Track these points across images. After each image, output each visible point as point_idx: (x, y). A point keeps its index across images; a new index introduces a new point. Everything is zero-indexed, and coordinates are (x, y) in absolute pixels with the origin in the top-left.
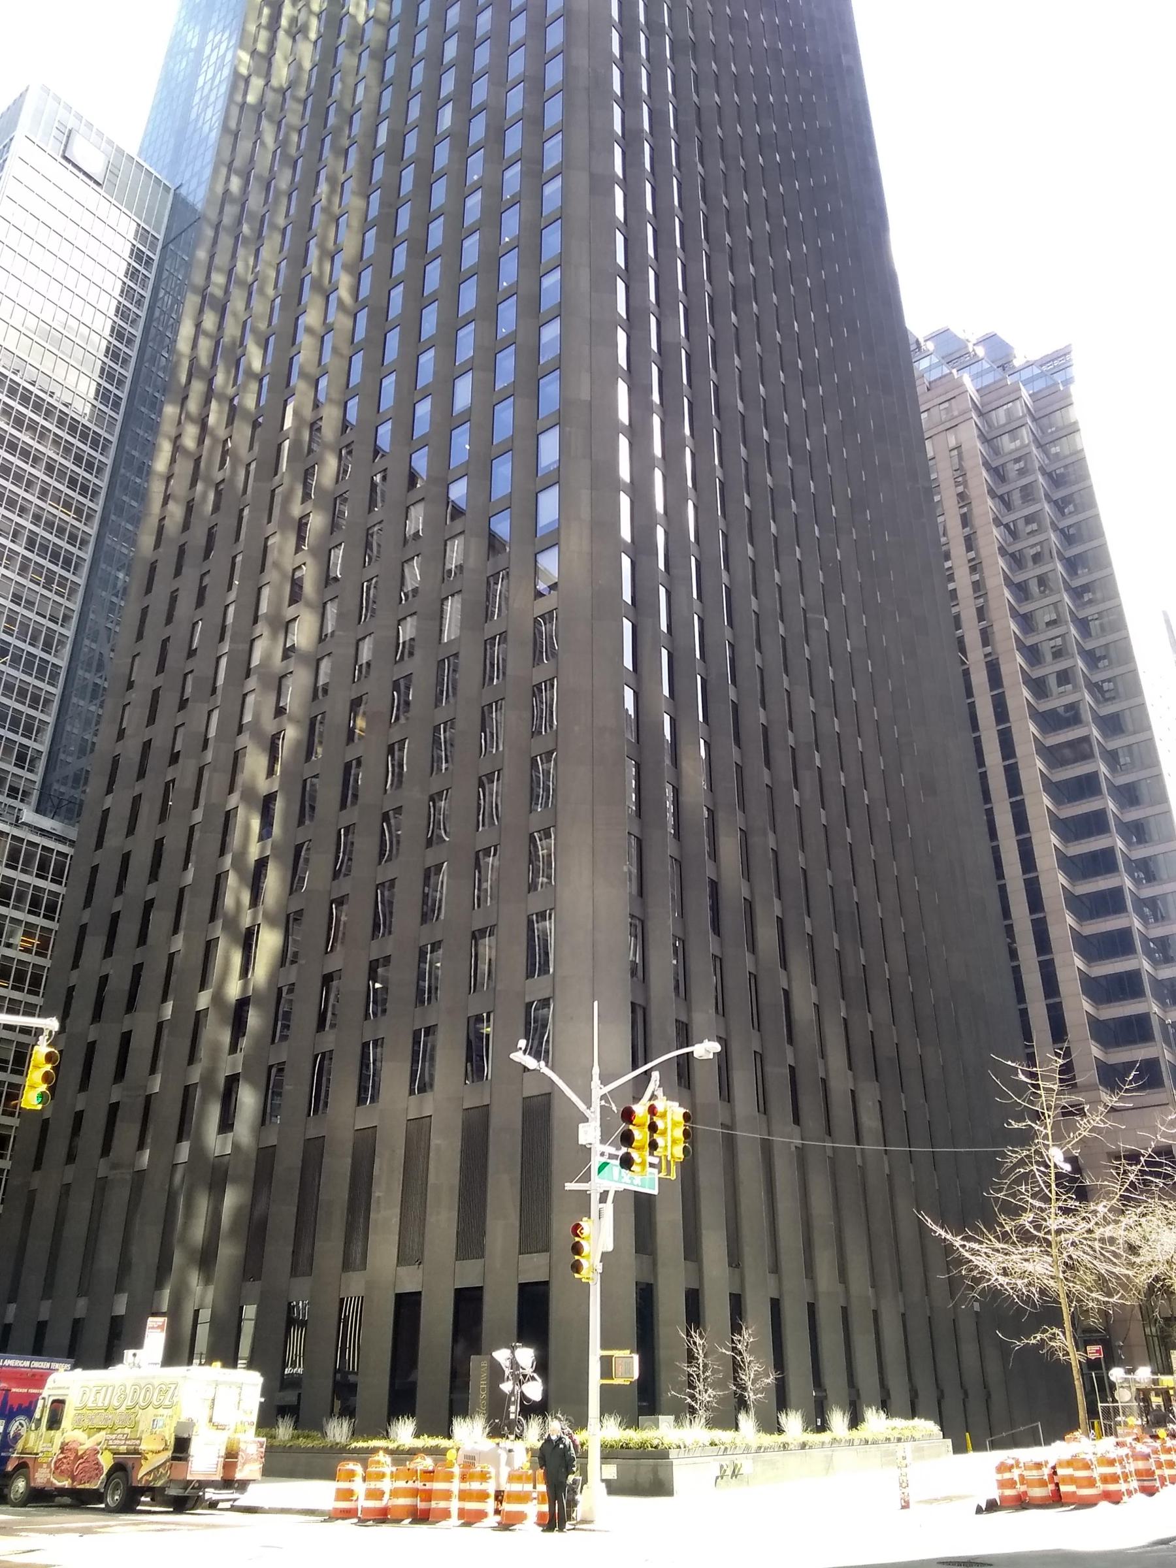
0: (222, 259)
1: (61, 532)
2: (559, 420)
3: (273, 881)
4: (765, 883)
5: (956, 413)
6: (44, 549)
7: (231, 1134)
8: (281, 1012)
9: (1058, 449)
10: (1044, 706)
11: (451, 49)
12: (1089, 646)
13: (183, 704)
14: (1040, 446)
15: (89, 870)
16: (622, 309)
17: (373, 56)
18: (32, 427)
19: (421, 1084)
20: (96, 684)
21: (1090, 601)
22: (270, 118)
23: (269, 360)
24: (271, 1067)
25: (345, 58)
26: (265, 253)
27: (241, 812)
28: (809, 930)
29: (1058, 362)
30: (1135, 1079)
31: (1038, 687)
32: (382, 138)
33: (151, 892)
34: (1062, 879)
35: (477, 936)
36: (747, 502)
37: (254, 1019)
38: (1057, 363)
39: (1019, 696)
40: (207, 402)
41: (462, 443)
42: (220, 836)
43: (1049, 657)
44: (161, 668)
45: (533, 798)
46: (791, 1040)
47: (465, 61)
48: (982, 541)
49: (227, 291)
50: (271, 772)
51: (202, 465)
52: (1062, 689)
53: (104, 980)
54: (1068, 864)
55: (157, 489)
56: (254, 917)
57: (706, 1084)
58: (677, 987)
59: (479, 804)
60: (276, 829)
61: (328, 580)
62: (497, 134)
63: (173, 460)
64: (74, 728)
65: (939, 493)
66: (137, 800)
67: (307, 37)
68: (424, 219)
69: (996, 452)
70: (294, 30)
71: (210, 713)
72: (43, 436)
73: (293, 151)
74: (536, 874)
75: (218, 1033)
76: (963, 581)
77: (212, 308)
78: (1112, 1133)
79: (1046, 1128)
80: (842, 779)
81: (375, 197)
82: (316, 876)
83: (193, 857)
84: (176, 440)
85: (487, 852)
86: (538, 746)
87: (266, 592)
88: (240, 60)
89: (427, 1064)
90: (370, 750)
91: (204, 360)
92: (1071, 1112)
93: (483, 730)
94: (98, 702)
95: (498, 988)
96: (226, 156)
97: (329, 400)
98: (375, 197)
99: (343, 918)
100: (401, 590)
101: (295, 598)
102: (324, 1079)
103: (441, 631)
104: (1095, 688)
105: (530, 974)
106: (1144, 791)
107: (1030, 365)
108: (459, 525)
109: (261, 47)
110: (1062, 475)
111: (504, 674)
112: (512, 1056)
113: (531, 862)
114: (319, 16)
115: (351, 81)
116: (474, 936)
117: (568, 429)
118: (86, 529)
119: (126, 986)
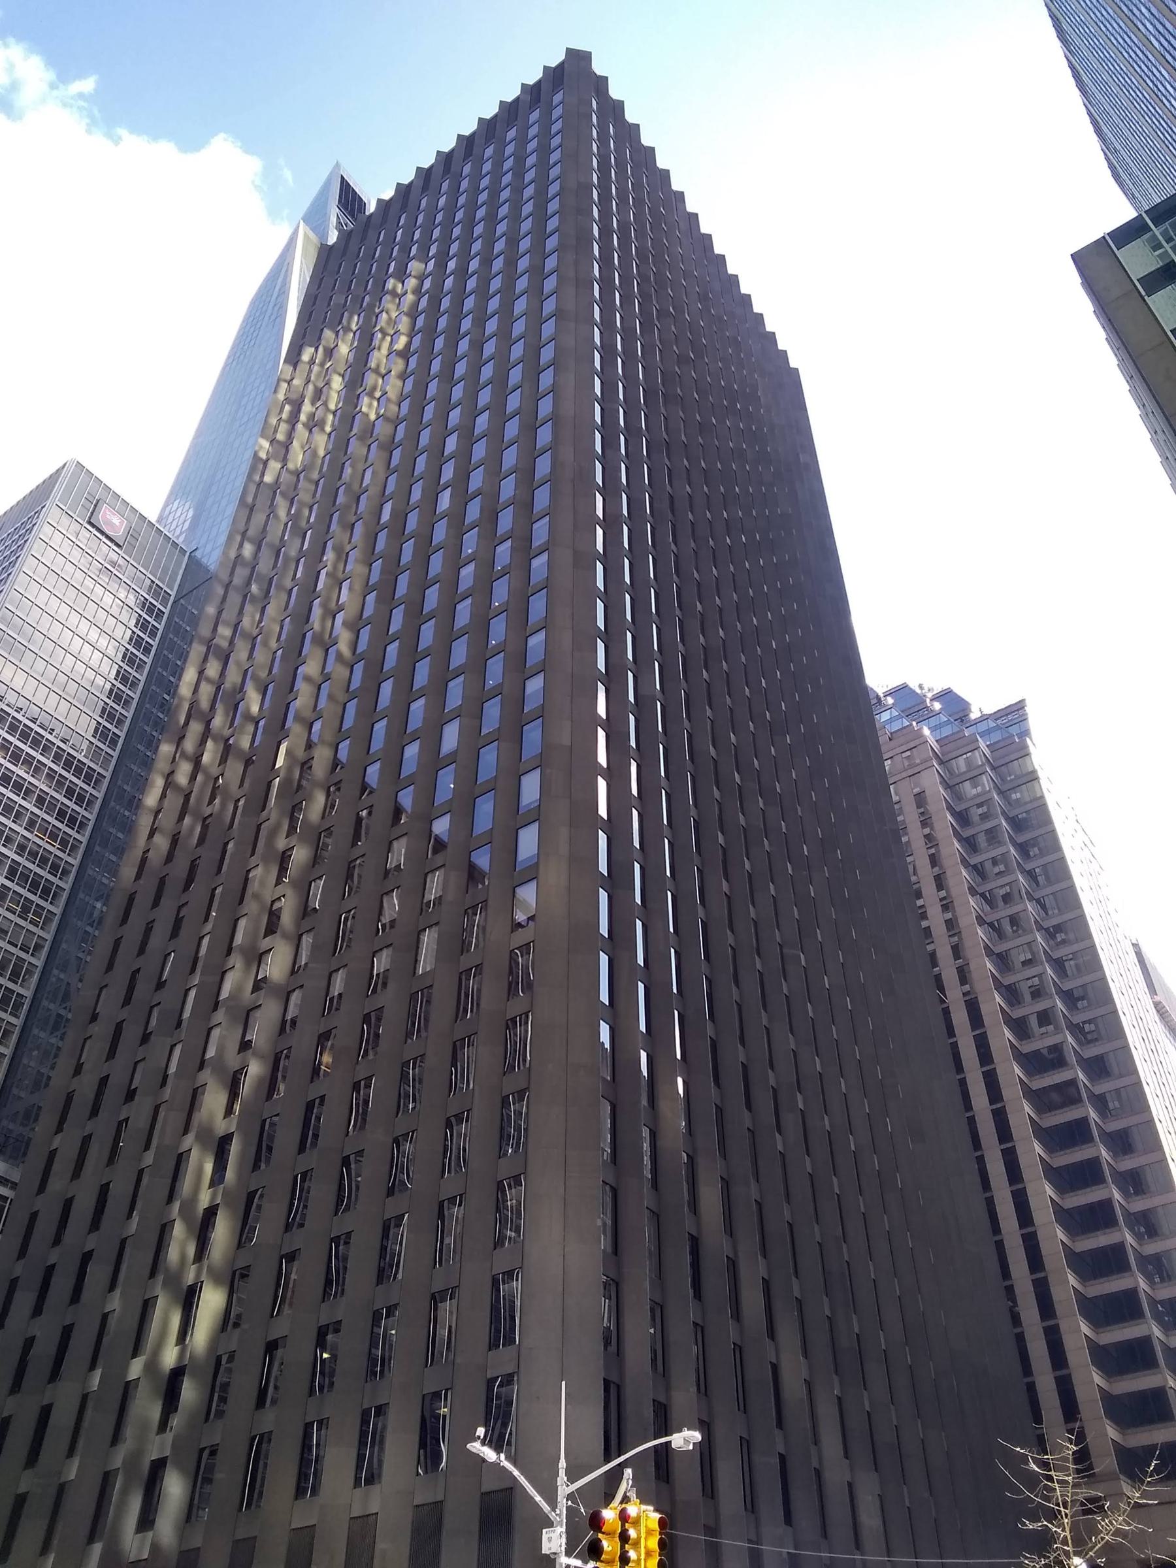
0: (229, 614)
1: (43, 862)
2: (540, 763)
3: (222, 1232)
4: (748, 1244)
5: (918, 761)
6: (24, 878)
7: (150, 1534)
8: (218, 1383)
9: (1018, 795)
10: (1027, 1048)
11: (451, 444)
12: (1067, 986)
13: (145, 1038)
14: (1001, 793)
15: (28, 1216)
16: (601, 666)
17: (381, 447)
18: (28, 761)
19: (367, 1474)
20: (59, 1015)
21: (1064, 942)
22: (283, 494)
23: (267, 705)
24: (202, 1450)
25: (355, 447)
26: (271, 610)
27: (194, 1154)
28: (797, 1293)
29: (1014, 715)
30: (1157, 1470)
31: (1020, 1027)
32: (386, 516)
33: (91, 1243)
34: (1061, 1234)
35: (437, 1298)
36: (721, 839)
37: (189, 1392)
38: (1013, 717)
39: (1002, 1037)
40: (202, 743)
41: (447, 783)
42: (170, 1181)
43: (1027, 997)
44: (127, 1001)
45: (503, 1137)
46: (780, 1424)
47: (465, 453)
48: (951, 881)
49: (231, 642)
50: (229, 1111)
51: (192, 800)
52: (1043, 1030)
53: (29, 1343)
54: (1065, 1217)
55: (144, 822)
56: (199, 1273)
57: (687, 1479)
58: (654, 1361)
59: (446, 1146)
60: (230, 1174)
61: (305, 911)
62: (491, 516)
63: (163, 796)
64: (31, 1061)
65: (906, 834)
66: (87, 1140)
67: (323, 430)
68: (422, 585)
69: (959, 797)
70: (311, 424)
71: (173, 1047)
72: (38, 769)
73: (303, 524)
74: (504, 1225)
75: (147, 1407)
76: (936, 919)
77: (217, 657)
78: (1137, 1538)
79: (1064, 1530)
80: (827, 1123)
81: (377, 565)
82: (266, 1230)
83: (139, 1205)
84: (169, 777)
85: (452, 1200)
86: (511, 1084)
87: (242, 923)
88: (261, 447)
89: (376, 1448)
90: (334, 1089)
91: (205, 704)
92: (1093, 1507)
93: (454, 1064)
94: (59, 1033)
95: (458, 1361)
96: (242, 527)
97: (322, 741)
98: (377, 565)
99: (293, 1276)
100: (379, 920)
101: (271, 930)
102: (261, 1463)
103: (416, 961)
104: (1077, 1029)
105: (493, 1345)
106: (1136, 1138)
107: (984, 718)
108: (440, 859)
109: (280, 437)
110: (1025, 819)
111: (478, 1005)
112: (469, 1446)
113: (498, 1209)
114: (334, 413)
115: (361, 467)
116: (433, 1297)
117: (548, 771)
118: (70, 860)
119: (53, 1350)
